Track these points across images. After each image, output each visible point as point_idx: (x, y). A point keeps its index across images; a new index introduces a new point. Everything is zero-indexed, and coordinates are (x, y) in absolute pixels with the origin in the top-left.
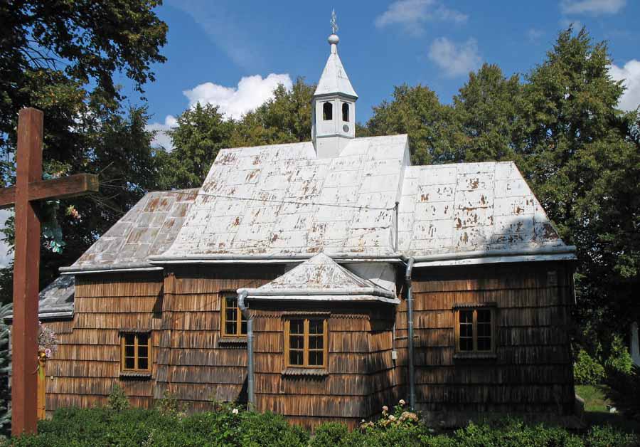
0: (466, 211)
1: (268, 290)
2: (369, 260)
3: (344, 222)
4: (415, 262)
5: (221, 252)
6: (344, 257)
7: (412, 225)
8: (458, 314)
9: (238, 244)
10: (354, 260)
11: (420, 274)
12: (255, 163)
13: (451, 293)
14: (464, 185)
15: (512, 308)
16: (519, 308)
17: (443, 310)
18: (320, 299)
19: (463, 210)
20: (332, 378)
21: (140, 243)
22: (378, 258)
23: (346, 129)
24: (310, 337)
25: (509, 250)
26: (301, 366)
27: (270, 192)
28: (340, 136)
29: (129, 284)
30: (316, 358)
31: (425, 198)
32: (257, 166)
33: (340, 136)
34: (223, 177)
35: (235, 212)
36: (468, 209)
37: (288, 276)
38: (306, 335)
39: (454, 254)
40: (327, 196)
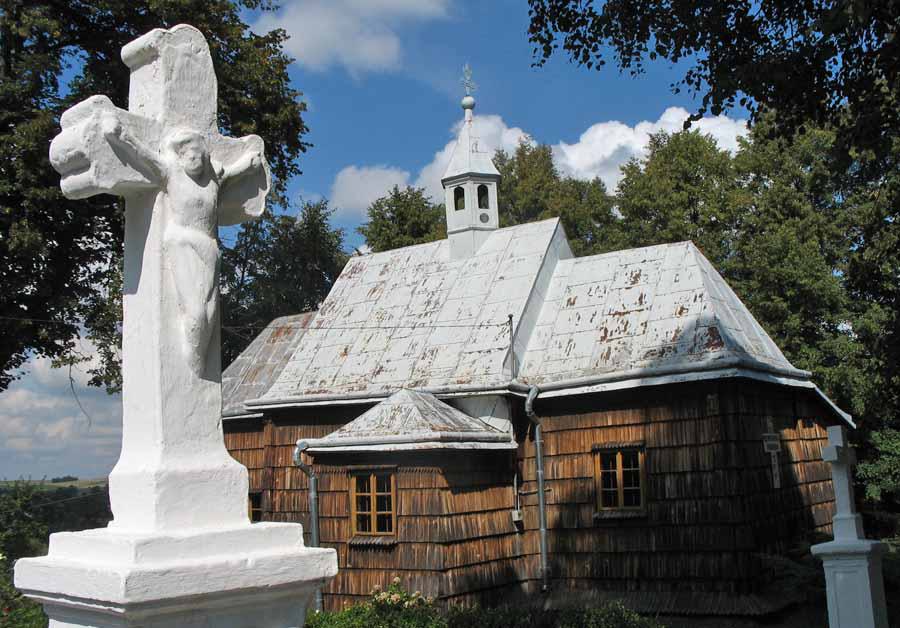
0: (617, 316)
1: (337, 440)
2: (473, 393)
3: (459, 345)
4: (540, 391)
5: (319, 392)
6: (446, 391)
7: (549, 340)
8: (598, 458)
9: (340, 380)
10: (457, 394)
11: (546, 407)
12: (382, 273)
13: (589, 431)
14: (623, 280)
15: (665, 448)
16: (673, 447)
17: (580, 453)
18: (403, 449)
19: (614, 315)
20: (401, 548)
21: (254, 384)
22: (484, 390)
23: (484, 218)
24: (378, 497)
25: (680, 366)
26: (369, 533)
27: (389, 310)
28: (475, 229)
29: (631, 411)
30: (384, 523)
31: (571, 303)
32: (383, 278)
33: (475, 229)
34: (345, 295)
35: (346, 338)
36: (620, 314)
37: (361, 422)
38: (373, 494)
39: (585, 379)
40: (447, 314)
